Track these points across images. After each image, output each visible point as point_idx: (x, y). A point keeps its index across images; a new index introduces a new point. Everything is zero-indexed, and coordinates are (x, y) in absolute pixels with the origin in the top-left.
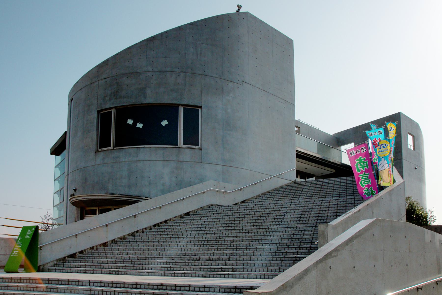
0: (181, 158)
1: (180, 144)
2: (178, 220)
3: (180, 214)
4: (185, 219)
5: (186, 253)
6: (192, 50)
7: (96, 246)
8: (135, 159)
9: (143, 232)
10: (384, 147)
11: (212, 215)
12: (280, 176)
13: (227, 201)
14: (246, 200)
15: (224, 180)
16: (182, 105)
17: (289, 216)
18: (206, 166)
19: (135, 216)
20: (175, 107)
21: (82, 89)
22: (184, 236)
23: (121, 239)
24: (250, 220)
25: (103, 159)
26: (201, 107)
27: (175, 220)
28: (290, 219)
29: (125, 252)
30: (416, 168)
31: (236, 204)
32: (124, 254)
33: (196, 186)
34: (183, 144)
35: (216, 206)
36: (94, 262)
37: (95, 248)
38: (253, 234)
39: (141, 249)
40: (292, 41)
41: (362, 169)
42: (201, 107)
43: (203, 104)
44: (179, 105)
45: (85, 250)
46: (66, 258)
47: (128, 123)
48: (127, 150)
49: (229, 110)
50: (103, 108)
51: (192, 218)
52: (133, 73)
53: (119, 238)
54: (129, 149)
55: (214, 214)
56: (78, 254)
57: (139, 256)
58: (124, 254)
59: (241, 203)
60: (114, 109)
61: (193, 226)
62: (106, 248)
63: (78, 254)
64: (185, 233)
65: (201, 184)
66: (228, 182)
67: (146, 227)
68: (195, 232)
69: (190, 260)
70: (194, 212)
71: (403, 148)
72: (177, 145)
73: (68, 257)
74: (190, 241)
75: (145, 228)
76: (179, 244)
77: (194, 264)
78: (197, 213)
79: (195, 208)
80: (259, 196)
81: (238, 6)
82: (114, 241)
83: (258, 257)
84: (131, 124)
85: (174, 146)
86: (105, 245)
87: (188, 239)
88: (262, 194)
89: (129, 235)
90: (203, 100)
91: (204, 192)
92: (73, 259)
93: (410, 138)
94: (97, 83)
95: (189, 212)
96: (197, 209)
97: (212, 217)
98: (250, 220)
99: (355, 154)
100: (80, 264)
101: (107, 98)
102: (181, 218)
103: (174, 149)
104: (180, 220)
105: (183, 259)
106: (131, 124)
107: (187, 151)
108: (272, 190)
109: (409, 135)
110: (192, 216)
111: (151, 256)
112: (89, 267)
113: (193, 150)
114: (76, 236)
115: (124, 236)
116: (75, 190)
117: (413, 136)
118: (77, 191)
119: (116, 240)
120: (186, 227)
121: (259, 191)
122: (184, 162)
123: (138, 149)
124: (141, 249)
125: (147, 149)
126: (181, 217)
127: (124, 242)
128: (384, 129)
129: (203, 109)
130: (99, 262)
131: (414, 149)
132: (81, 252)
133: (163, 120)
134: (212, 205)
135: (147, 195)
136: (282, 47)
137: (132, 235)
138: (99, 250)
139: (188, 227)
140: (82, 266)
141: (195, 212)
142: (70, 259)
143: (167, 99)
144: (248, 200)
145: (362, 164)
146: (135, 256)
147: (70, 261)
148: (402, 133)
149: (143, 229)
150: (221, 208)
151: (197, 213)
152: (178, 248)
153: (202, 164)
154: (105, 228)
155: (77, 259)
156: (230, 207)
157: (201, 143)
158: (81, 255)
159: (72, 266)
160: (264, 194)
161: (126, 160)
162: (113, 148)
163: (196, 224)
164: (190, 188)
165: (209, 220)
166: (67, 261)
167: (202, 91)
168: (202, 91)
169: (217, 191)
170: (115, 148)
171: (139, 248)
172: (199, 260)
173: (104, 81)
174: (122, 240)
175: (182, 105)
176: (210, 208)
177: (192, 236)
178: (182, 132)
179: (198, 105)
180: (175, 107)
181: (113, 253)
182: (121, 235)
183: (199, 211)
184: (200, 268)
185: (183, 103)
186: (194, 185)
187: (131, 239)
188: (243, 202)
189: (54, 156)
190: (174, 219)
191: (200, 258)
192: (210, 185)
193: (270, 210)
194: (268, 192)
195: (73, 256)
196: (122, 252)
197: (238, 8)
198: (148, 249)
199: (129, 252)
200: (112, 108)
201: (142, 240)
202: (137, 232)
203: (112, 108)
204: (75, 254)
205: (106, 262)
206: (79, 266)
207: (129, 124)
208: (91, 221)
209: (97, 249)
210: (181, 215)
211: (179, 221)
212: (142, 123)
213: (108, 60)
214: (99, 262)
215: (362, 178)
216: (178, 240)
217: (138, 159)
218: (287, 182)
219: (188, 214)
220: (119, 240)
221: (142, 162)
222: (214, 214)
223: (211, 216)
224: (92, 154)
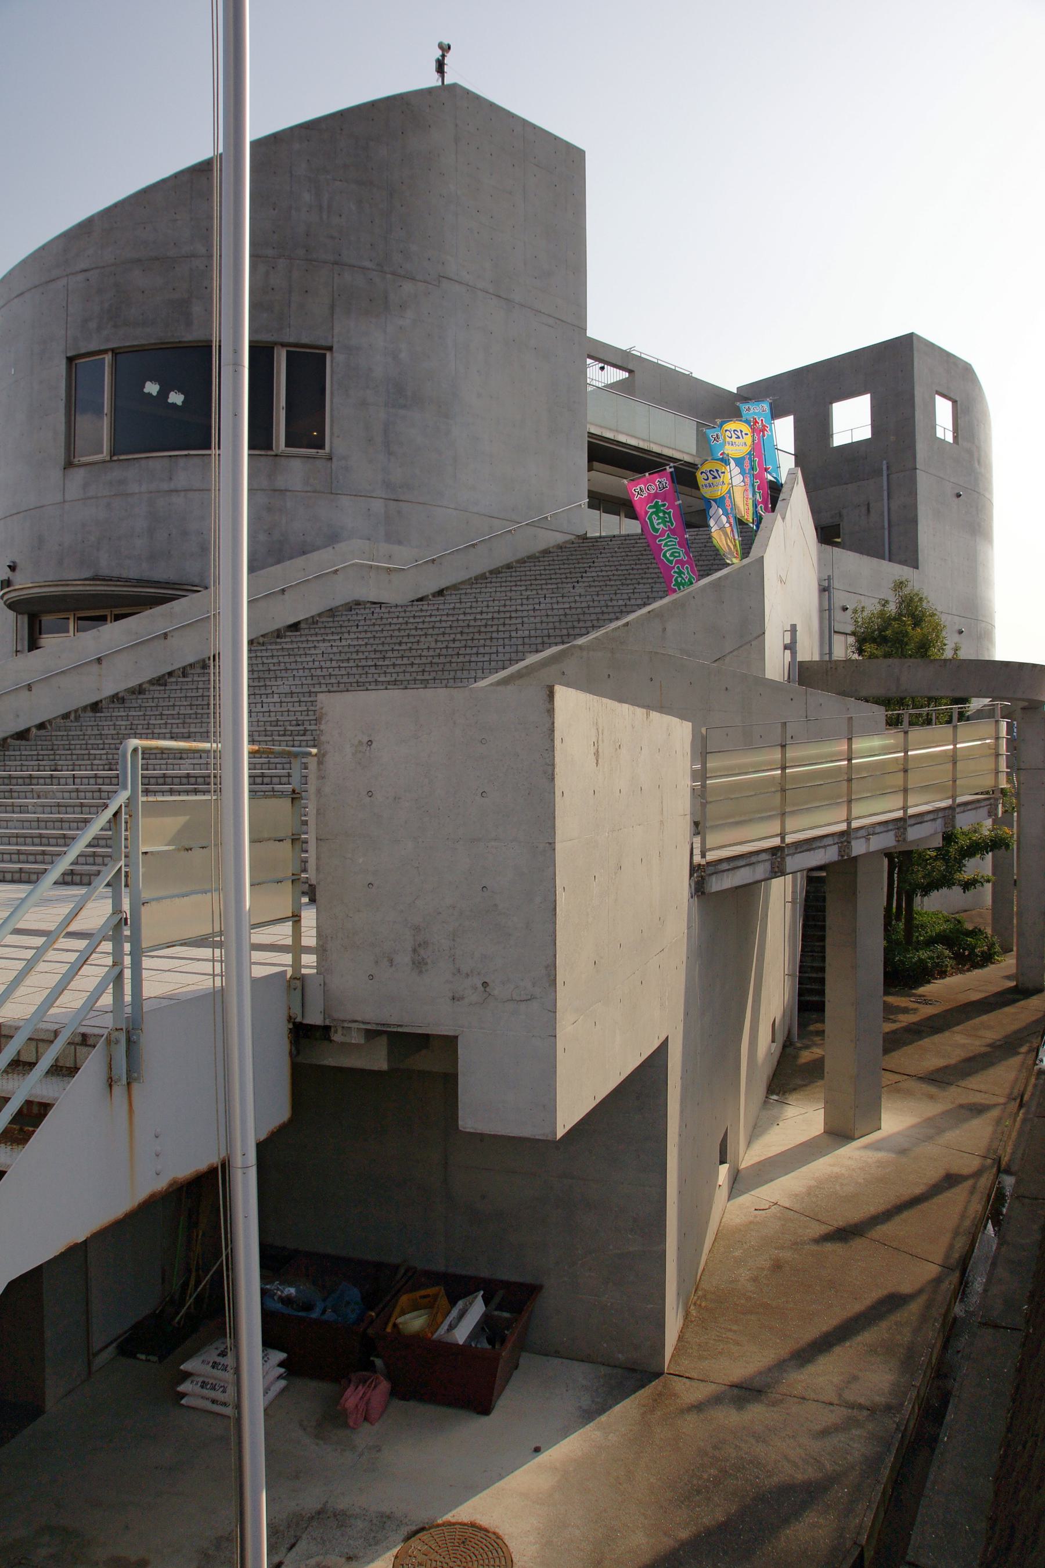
0: (281, 483)
1: (278, 446)
2: (271, 644)
3: (276, 627)
4: (286, 643)
5: (278, 721)
6: (307, 197)
7: (76, 711)
8: (165, 486)
10: (715, 478)
11: (354, 629)
12: (541, 524)
13: (394, 592)
14: (447, 588)
15: (389, 538)
16: (283, 345)
18: (345, 501)
19: (165, 636)
22: (279, 682)
23: (133, 693)
24: (436, 641)
25: (86, 486)
26: (330, 349)
27: (263, 644)
29: (142, 722)
30: (959, 496)
31: (421, 599)
32: (140, 727)
33: (315, 556)
34: (287, 446)
35: (368, 605)
36: (72, 747)
37: (72, 717)
39: (179, 714)
40: (581, 154)
41: (661, 526)
42: (330, 349)
43: (335, 339)
44: (276, 343)
45: (50, 721)
46: (9, 740)
47: (146, 390)
48: (143, 462)
49: (403, 355)
50: (83, 351)
51: (304, 638)
52: (157, 259)
53: (127, 690)
54: (151, 462)
55: (357, 626)
56: (34, 730)
57: (175, 730)
58: (140, 727)
59: (434, 595)
60: (110, 354)
61: (303, 659)
62: (98, 715)
63: (34, 730)
64: (284, 674)
65: (330, 549)
66: (400, 543)
67: (192, 660)
68: (307, 673)
69: (284, 735)
70: (310, 621)
72: (271, 449)
73: (12, 737)
74: (292, 693)
75: (191, 665)
76: (265, 700)
77: (291, 743)
78: (320, 625)
79: (314, 611)
80: (483, 576)
81: (441, 46)
82: (117, 699)
84: (155, 394)
85: (263, 453)
86: (95, 707)
87: (287, 689)
88: (491, 572)
89: (151, 682)
90: (336, 331)
91: (337, 570)
92: (23, 742)
93: (943, 409)
94: (64, 281)
95: (299, 623)
96: (320, 615)
97: (352, 636)
98: (436, 641)
99: (645, 494)
100: (41, 752)
101: (93, 325)
102: (278, 637)
103: (262, 458)
104: (276, 643)
105: (269, 733)
106: (155, 394)
107: (296, 464)
108: (518, 562)
109: (939, 399)
110: (306, 632)
111: (201, 730)
112: (63, 757)
113: (311, 460)
114: (29, 687)
115: (140, 685)
117: (954, 402)
119: (120, 695)
120: (287, 659)
121: (480, 564)
122: (288, 493)
123: (173, 459)
124: (179, 714)
125: (196, 460)
126: (278, 634)
127: (139, 701)
128: (771, 404)
129: (335, 355)
130: (84, 747)
131: (955, 438)
132: (41, 726)
134: (358, 603)
135: (197, 581)
136: (554, 170)
137: (160, 681)
138: (82, 719)
139: (292, 659)
140: (46, 757)
141: (313, 621)
142: (18, 742)
144: (455, 587)
145: (661, 515)
146: (164, 731)
147: (17, 748)
149: (184, 668)
150: (378, 610)
151: (320, 625)
152: (263, 710)
153: (332, 496)
154: (95, 667)
155: (33, 743)
156: (399, 609)
157: (331, 443)
158: (42, 732)
159: (24, 758)
161: (144, 488)
162: (108, 458)
163: (313, 651)
164: (300, 562)
165: (344, 643)
166: (11, 748)
167: (332, 307)
168: (332, 307)
169: (371, 567)
170: (115, 458)
171: (175, 712)
172: (304, 735)
173: (80, 277)
174: (134, 696)
175: (283, 345)
176: (353, 612)
177: (297, 682)
178: (283, 414)
181: (114, 725)
182: (133, 683)
183: (324, 619)
186: (314, 550)
187: (157, 691)
188: (440, 593)
190: (261, 640)
191: (306, 730)
192: (352, 552)
194: (509, 566)
195: (22, 735)
196: (136, 722)
197: (440, 53)
198: (196, 714)
199: (151, 722)
200: (105, 351)
201: (183, 695)
203: (105, 351)
204: (28, 730)
205: (101, 746)
206: (40, 757)
207: (149, 394)
208: (67, 646)
209: (77, 718)
210: (278, 630)
211: (273, 647)
212: (181, 390)
213: (89, 222)
214: (84, 747)
215: (666, 545)
216: (263, 692)
217: (172, 486)
219: (295, 627)
220: (127, 696)
221: (183, 494)
222: (357, 626)
223: (349, 632)
224: (56, 473)
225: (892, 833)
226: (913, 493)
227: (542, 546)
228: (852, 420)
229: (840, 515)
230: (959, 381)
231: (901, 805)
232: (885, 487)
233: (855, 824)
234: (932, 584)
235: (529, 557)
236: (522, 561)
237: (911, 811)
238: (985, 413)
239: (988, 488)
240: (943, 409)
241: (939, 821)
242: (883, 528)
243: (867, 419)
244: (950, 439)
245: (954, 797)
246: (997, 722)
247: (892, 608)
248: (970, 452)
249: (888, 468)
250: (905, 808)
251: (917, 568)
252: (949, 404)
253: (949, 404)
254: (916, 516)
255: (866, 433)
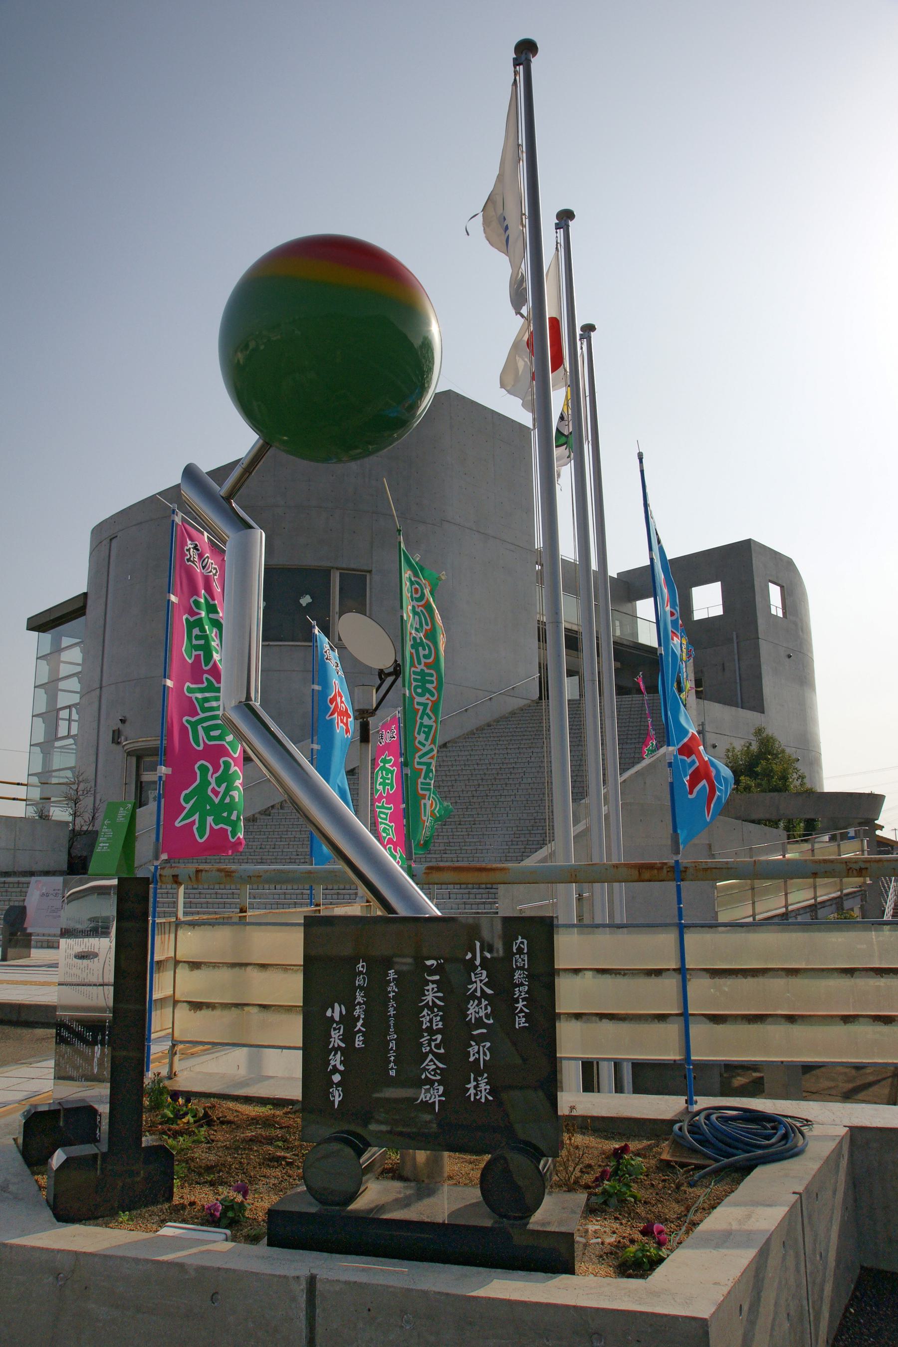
9: (282, 807)
16: (337, 569)
17: (529, 780)
20: (326, 573)
21: (141, 523)
28: (532, 785)
30: (789, 656)
38: (474, 812)
42: (370, 572)
71: (758, 614)
83: (487, 847)
88: (477, 729)
93: (775, 592)
108: (494, 721)
109: (771, 585)
116: (123, 721)
117: (782, 587)
118: (127, 724)
131: (784, 613)
133: (302, 594)
137: (266, 812)
143: (309, 560)
148: (756, 583)
149: (282, 803)
160: (480, 729)
179: (366, 568)
180: (326, 573)
184: (285, 894)
185: (340, 566)
189: (35, 634)
193: (497, 766)
194: (489, 725)
202: (273, 807)
218: (522, 703)
225: (834, 906)
226: (757, 656)
227: (510, 709)
228: (708, 601)
229: (702, 671)
230: (785, 571)
231: (783, 904)
232: (736, 651)
233: (790, 908)
234: (776, 723)
235: (501, 718)
236: (497, 721)
237: (819, 899)
238: (804, 593)
239: (810, 650)
240: (775, 592)
241: (834, 906)
242: (736, 682)
243: (719, 601)
244: (780, 614)
245: (841, 890)
246: (862, 841)
247: (754, 747)
248: (795, 624)
249: (737, 637)
250: (815, 898)
251: (763, 713)
252: (778, 588)
253: (778, 588)
254: (761, 674)
255: (718, 611)
